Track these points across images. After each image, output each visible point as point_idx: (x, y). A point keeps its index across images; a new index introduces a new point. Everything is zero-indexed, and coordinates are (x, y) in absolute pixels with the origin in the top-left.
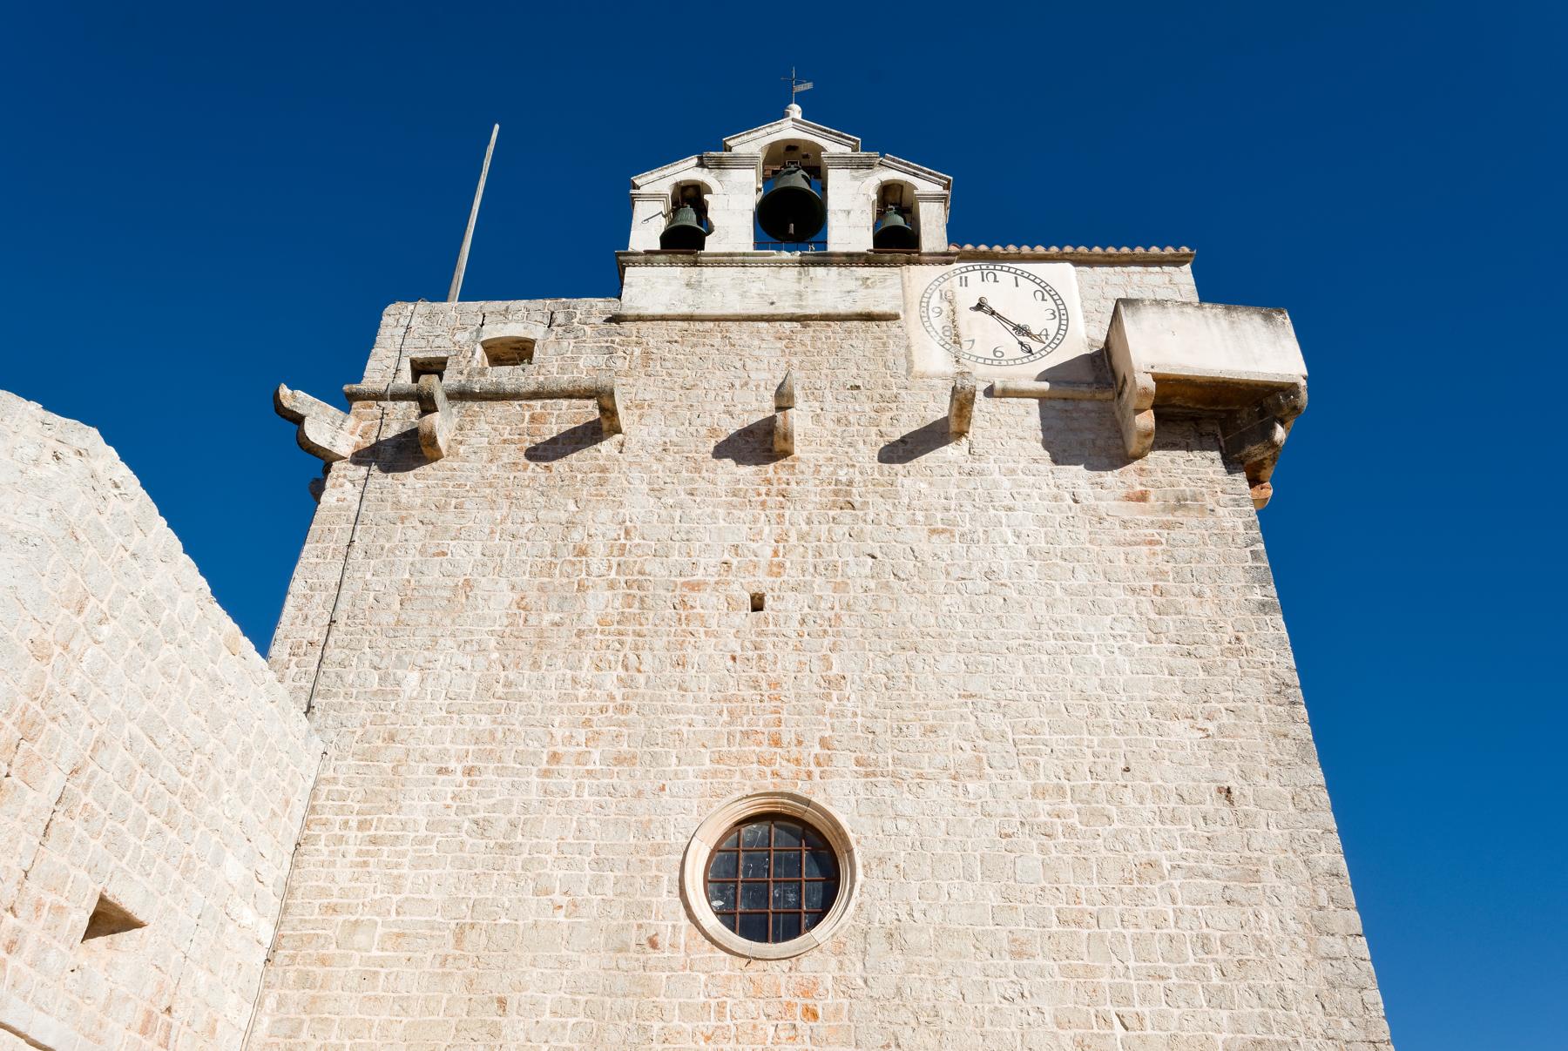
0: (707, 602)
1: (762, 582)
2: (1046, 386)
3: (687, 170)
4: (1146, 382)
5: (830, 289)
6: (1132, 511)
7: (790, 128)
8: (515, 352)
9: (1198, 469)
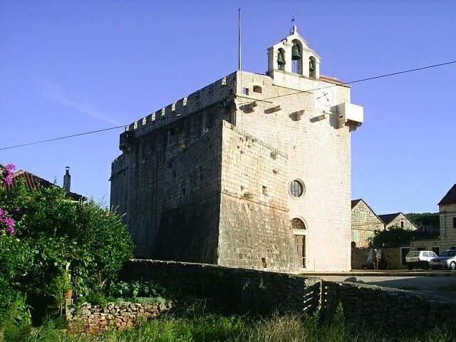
0: (289, 147)
1: (295, 144)
2: (331, 113)
3: (280, 45)
4: (346, 121)
5: (306, 84)
6: (337, 138)
7: (296, 36)
8: (257, 89)
9: (346, 129)
